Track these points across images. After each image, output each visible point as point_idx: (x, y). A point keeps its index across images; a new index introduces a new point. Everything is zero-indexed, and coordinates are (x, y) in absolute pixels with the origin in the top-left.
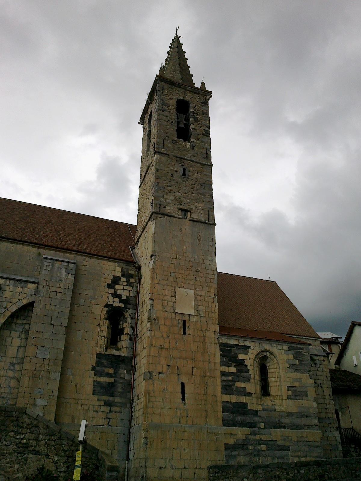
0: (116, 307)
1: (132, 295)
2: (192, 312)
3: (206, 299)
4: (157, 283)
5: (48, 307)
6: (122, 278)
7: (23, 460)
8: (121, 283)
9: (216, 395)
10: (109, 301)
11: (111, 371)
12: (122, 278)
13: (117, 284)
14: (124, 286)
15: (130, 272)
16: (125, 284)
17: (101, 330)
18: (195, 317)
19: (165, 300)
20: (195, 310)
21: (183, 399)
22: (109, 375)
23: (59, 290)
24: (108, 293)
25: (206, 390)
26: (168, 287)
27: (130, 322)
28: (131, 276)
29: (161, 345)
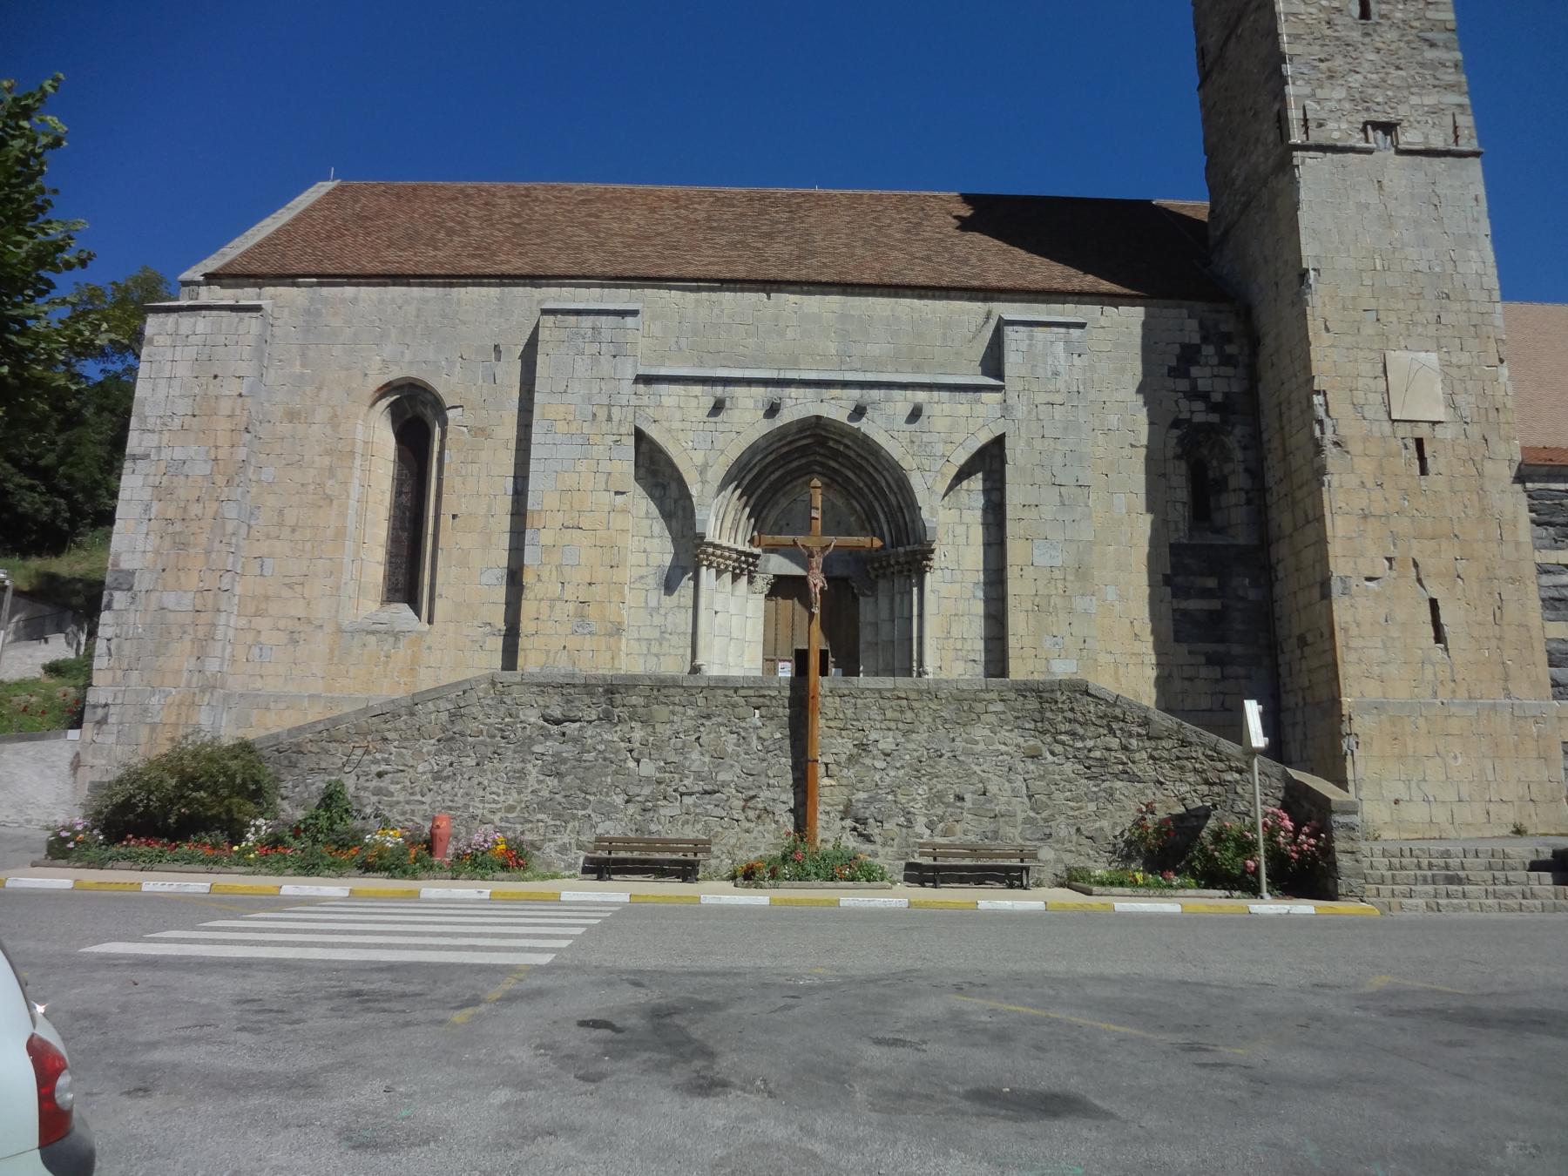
0: (1199, 424)
1: (1236, 388)
2: (1439, 413)
3: (1476, 372)
4: (1330, 347)
5: (1038, 444)
6: (1204, 347)
7: (926, 788)
8: (1203, 361)
9: (1530, 624)
10: (1180, 412)
11: (1211, 583)
12: (1204, 347)
13: (1193, 365)
14: (1212, 366)
15: (1224, 328)
16: (1215, 360)
17: (1170, 488)
18: (1449, 425)
19: (1357, 390)
20: (1446, 407)
21: (1439, 637)
22: (1206, 593)
23: (1058, 399)
24: (1175, 391)
25: (1498, 615)
26: (1361, 354)
27: (1241, 459)
28: (1228, 338)
29: (1362, 510)
